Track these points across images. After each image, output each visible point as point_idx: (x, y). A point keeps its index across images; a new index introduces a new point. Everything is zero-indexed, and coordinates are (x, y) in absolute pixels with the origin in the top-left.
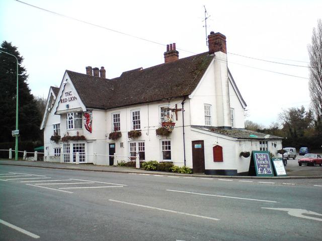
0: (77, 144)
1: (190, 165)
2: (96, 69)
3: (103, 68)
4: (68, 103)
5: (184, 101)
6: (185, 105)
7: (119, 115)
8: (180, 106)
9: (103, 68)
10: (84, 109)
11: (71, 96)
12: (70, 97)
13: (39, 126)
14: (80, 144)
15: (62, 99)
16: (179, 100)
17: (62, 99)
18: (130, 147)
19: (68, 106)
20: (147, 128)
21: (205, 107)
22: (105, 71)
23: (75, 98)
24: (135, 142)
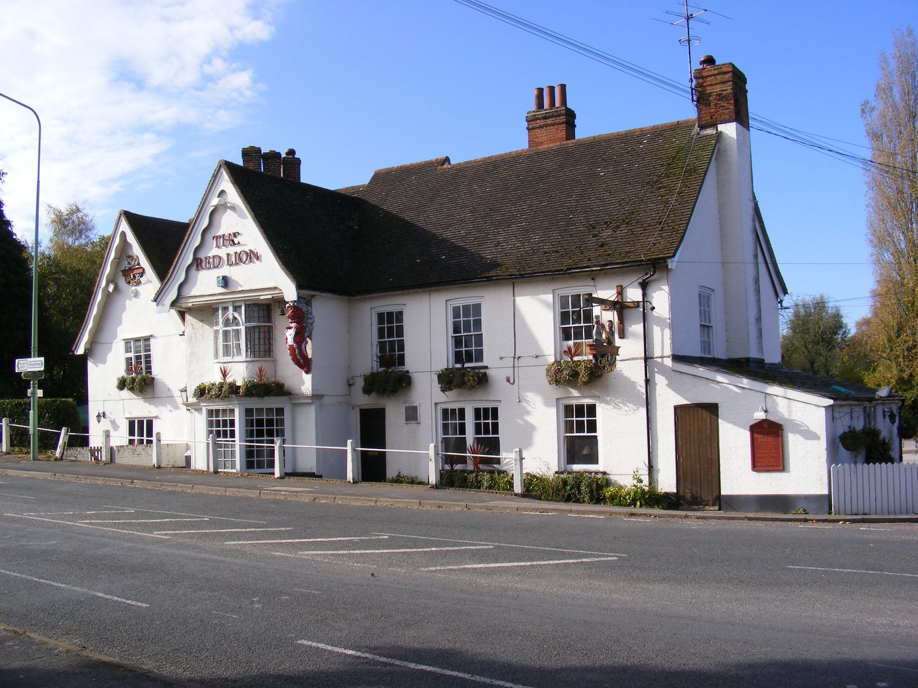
0: (260, 410)
1: (667, 483)
2: (275, 155)
3: (291, 152)
4: (225, 271)
5: (667, 275)
6: (650, 290)
7: (401, 313)
8: (634, 294)
9: (291, 152)
10: (290, 292)
11: (238, 249)
12: (232, 250)
13: (72, 347)
14: (270, 410)
15: (202, 255)
16: (635, 272)
17: (202, 255)
18: (440, 422)
19: (225, 282)
20: (510, 362)
21: (700, 295)
22: (298, 162)
23: (252, 256)
24: (461, 406)
